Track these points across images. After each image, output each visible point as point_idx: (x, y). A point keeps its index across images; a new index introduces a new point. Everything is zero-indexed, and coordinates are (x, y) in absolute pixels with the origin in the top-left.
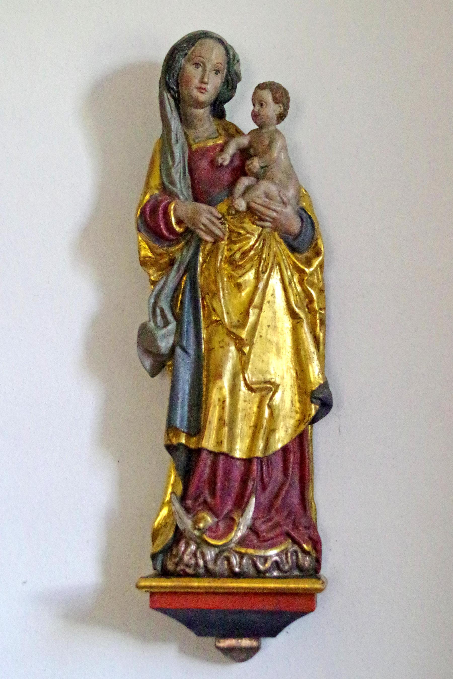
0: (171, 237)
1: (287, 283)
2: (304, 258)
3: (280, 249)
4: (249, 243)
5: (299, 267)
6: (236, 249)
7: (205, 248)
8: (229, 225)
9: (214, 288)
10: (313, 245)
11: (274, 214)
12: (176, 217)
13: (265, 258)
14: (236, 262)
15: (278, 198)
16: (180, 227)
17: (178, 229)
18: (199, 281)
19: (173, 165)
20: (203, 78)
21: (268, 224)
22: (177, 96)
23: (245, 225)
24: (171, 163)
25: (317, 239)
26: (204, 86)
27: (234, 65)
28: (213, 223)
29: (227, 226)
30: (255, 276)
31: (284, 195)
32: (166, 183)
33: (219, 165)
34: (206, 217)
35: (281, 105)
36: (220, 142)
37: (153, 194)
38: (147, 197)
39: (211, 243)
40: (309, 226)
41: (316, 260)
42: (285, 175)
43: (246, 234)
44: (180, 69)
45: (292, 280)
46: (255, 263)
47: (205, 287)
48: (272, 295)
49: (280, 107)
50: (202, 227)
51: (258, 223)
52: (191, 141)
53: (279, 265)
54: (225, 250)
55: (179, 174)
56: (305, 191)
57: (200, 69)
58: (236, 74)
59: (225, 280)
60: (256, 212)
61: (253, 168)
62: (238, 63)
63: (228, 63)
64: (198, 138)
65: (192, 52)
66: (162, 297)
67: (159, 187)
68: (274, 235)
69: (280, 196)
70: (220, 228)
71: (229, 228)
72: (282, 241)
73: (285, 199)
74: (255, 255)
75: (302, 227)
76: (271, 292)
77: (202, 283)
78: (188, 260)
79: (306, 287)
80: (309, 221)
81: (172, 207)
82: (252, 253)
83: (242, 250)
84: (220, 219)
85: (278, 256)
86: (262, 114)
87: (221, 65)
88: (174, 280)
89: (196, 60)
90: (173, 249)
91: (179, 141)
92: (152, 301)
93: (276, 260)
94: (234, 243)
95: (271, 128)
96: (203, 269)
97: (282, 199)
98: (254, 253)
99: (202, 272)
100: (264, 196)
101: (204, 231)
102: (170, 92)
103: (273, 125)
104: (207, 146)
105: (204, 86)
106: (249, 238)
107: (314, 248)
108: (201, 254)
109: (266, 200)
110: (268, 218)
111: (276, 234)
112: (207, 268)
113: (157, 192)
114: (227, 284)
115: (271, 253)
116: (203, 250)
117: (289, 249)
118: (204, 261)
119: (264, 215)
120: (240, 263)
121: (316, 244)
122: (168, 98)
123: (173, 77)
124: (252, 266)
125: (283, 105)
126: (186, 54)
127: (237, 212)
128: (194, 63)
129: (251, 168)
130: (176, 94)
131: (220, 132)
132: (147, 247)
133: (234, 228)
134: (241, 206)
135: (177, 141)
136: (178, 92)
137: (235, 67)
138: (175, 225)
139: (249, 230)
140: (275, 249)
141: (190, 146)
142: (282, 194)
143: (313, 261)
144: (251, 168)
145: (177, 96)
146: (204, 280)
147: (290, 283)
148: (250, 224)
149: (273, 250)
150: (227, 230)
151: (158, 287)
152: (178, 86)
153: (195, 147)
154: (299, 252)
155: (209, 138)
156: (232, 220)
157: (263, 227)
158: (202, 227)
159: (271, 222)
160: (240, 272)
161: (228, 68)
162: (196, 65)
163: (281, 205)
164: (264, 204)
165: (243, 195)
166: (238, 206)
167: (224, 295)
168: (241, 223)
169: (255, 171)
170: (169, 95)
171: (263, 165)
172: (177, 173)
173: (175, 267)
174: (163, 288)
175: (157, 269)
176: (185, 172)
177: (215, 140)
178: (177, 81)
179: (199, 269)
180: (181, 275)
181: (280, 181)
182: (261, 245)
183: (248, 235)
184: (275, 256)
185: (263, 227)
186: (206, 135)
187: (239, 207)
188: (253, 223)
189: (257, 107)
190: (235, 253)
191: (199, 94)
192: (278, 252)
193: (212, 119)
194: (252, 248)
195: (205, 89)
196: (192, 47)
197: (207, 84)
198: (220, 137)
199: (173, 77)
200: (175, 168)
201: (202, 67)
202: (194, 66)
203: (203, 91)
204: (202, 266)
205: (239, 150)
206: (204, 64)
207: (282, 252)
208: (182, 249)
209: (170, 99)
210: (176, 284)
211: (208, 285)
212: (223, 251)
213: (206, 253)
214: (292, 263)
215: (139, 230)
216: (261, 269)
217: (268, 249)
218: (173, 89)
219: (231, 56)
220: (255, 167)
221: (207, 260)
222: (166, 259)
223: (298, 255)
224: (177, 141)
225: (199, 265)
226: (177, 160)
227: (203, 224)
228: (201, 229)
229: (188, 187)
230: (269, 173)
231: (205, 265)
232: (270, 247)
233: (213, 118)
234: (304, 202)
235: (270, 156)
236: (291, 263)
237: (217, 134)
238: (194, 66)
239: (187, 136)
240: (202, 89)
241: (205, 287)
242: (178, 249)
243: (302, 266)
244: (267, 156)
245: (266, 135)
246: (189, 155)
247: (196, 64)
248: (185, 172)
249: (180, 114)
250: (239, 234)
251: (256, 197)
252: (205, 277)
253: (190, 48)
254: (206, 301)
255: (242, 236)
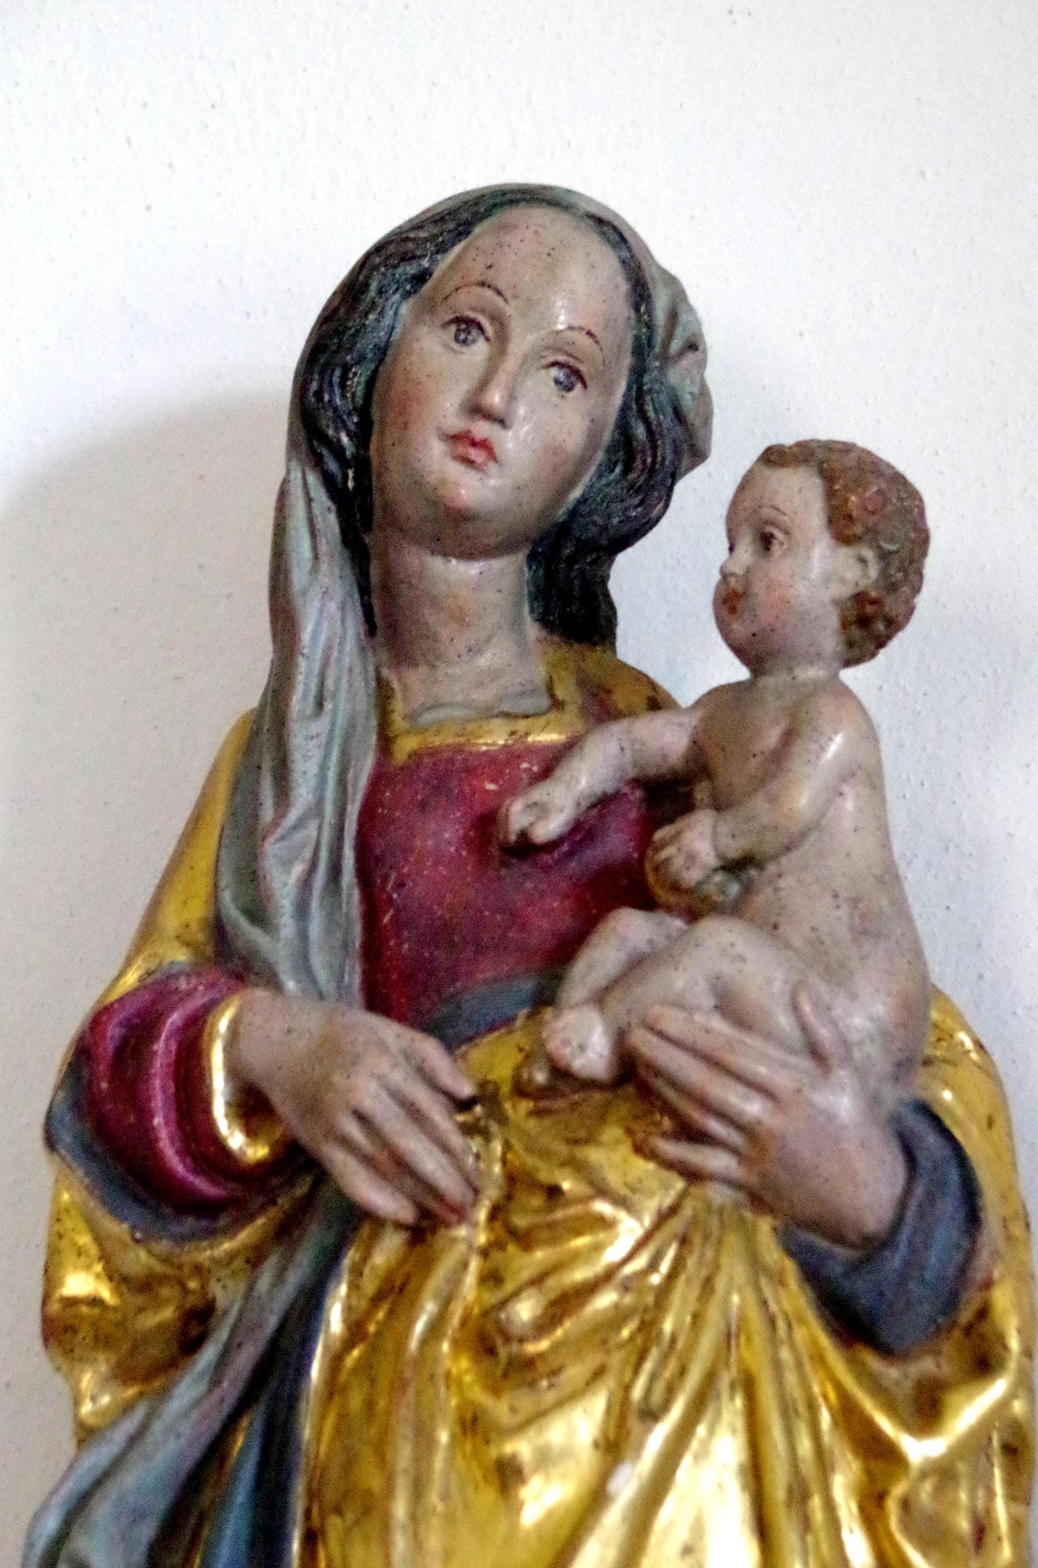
0: (202, 1184)
1: (778, 1490)
2: (908, 1385)
3: (773, 1307)
4: (597, 1248)
5: (869, 1424)
6: (526, 1275)
7: (365, 1259)
8: (507, 1146)
9: (376, 1484)
10: (965, 1316)
11: (753, 1108)
12: (233, 1071)
13: (673, 1340)
14: (508, 1339)
15: (784, 1021)
16: (251, 1133)
17: (235, 1139)
18: (307, 1433)
19: (276, 823)
20: (483, 385)
21: (717, 1161)
22: (351, 484)
23: (594, 1155)
24: (268, 813)
25: (988, 1284)
26: (482, 429)
27: (665, 358)
28: (414, 1113)
29: (497, 1147)
30: (604, 1432)
31: (823, 1009)
32: (232, 911)
33: (513, 838)
34: (381, 1078)
35: (869, 554)
36: (549, 737)
37: (161, 963)
38: (131, 979)
39: (399, 1226)
40: (949, 1206)
41: (971, 1397)
42: (843, 913)
43: (589, 1198)
44: (382, 351)
45: (814, 1487)
46: (616, 1360)
47: (334, 1471)
48: (687, 1550)
49: (863, 561)
50: (353, 1130)
51: (672, 1149)
52: (398, 723)
53: (748, 1386)
54: (470, 1279)
55: (298, 869)
56: (979, 1046)
57: (480, 350)
58: (679, 415)
59: (444, 1437)
60: (659, 1084)
61: (678, 862)
62: (691, 357)
63: (641, 349)
64: (437, 705)
65: (453, 267)
66: (102, 1510)
67: (200, 937)
68: (750, 1237)
69: (795, 1008)
70: (446, 1149)
71: (504, 1161)
72: (790, 1268)
73: (824, 1034)
74: (618, 1317)
75: (903, 1203)
76: (680, 1536)
77: (323, 1449)
78: (272, 1321)
79: (895, 1546)
80: (954, 1177)
81: (223, 1024)
82: (605, 1300)
83: (555, 1285)
84: (463, 1105)
85: (749, 1339)
86: (759, 588)
87: (587, 341)
88: (186, 1428)
89: (465, 302)
90: (206, 1253)
91: (328, 706)
92: (51, 1524)
93: (733, 1359)
94: (525, 1240)
95: (810, 673)
96: (343, 1377)
97: (804, 1028)
98: (617, 1306)
99: (333, 1386)
100: (709, 1002)
101: (368, 1161)
102: (318, 462)
103: (815, 657)
104: (474, 749)
105: (482, 429)
106: (604, 1224)
107: (968, 1330)
108: (343, 1289)
109: (719, 1024)
110: (715, 1126)
111: (765, 1227)
112: (366, 1367)
113: (181, 956)
114: (450, 1460)
115: (713, 1314)
116: (357, 1271)
117: (821, 1316)
118: (355, 1331)
119: (704, 1104)
120: (532, 1348)
121: (983, 1313)
122: (307, 493)
123: (343, 386)
124: (599, 1374)
125: (884, 556)
126: (421, 278)
127: (560, 1073)
128: (451, 316)
129: (667, 861)
130: (351, 473)
131: (560, 693)
132: (94, 1251)
133: (530, 1161)
134: (582, 1048)
135: (320, 704)
136: (362, 465)
137: (674, 376)
138: (227, 1116)
139: (613, 1179)
140: (735, 1299)
141: (386, 742)
142: (807, 1008)
143: (952, 1399)
144: (667, 861)
145: (351, 484)
146: (339, 1432)
147: (799, 1495)
148: (625, 1149)
149: (726, 1301)
150: (497, 1169)
151: (100, 1456)
152: (363, 434)
153: (406, 746)
154: (886, 1351)
155: (488, 713)
156: (532, 1124)
157: (693, 1175)
158: (353, 1130)
159: (735, 1151)
160: (526, 1402)
161: (638, 372)
162: (463, 326)
163: (805, 1063)
164: (704, 1042)
165: (600, 998)
166: (567, 1042)
167: (413, 1517)
168: (576, 1142)
169: (692, 876)
170: (313, 479)
171: (734, 849)
172: (287, 864)
173: (209, 1354)
174: (117, 1463)
175: (119, 1365)
176: (335, 870)
177: (522, 725)
178: (364, 412)
179: (316, 1370)
180: (231, 1400)
181: (817, 944)
182: (665, 1266)
183: (602, 1207)
184: (728, 1338)
185: (693, 1175)
186: (483, 696)
187: (567, 1051)
188: (639, 1149)
189: (746, 553)
190: (516, 1294)
191: (455, 470)
192: (755, 1318)
193: (533, 630)
194: (609, 1275)
195: (484, 445)
196: (454, 244)
197: (502, 422)
198: (551, 716)
199: (343, 386)
200: (283, 838)
201: (487, 339)
202: (453, 328)
203: (474, 454)
204: (335, 1362)
205: (637, 782)
206: (500, 321)
207: (781, 1324)
208: (255, 1258)
209: (313, 494)
210: (195, 1453)
211: (349, 1465)
212: (456, 1280)
213: (370, 1285)
214: (832, 1396)
215: (51, 1142)
216: (637, 1392)
217: (696, 1292)
218: (338, 451)
219: (660, 316)
220: (691, 858)
221: (372, 1328)
222: (168, 1314)
223: (873, 1362)
224: (320, 704)
225: (319, 1350)
226: (303, 794)
227: (362, 1118)
228: (345, 1142)
229: (345, 945)
230: (763, 897)
231: (356, 1353)
232: (708, 1286)
233: (544, 634)
234: (947, 1085)
235: (773, 800)
236: (826, 1398)
237: (545, 702)
238: (453, 328)
239: (383, 694)
240: (474, 444)
241: (334, 1471)
242: (232, 1256)
243: (885, 1423)
244: (759, 804)
245: (772, 704)
246: (379, 780)
247: (458, 320)
248: (335, 870)
249: (364, 589)
250: (553, 1192)
251: (662, 1002)
252: (343, 1416)
253: (442, 249)
254: (326, 1548)
255: (568, 1204)
